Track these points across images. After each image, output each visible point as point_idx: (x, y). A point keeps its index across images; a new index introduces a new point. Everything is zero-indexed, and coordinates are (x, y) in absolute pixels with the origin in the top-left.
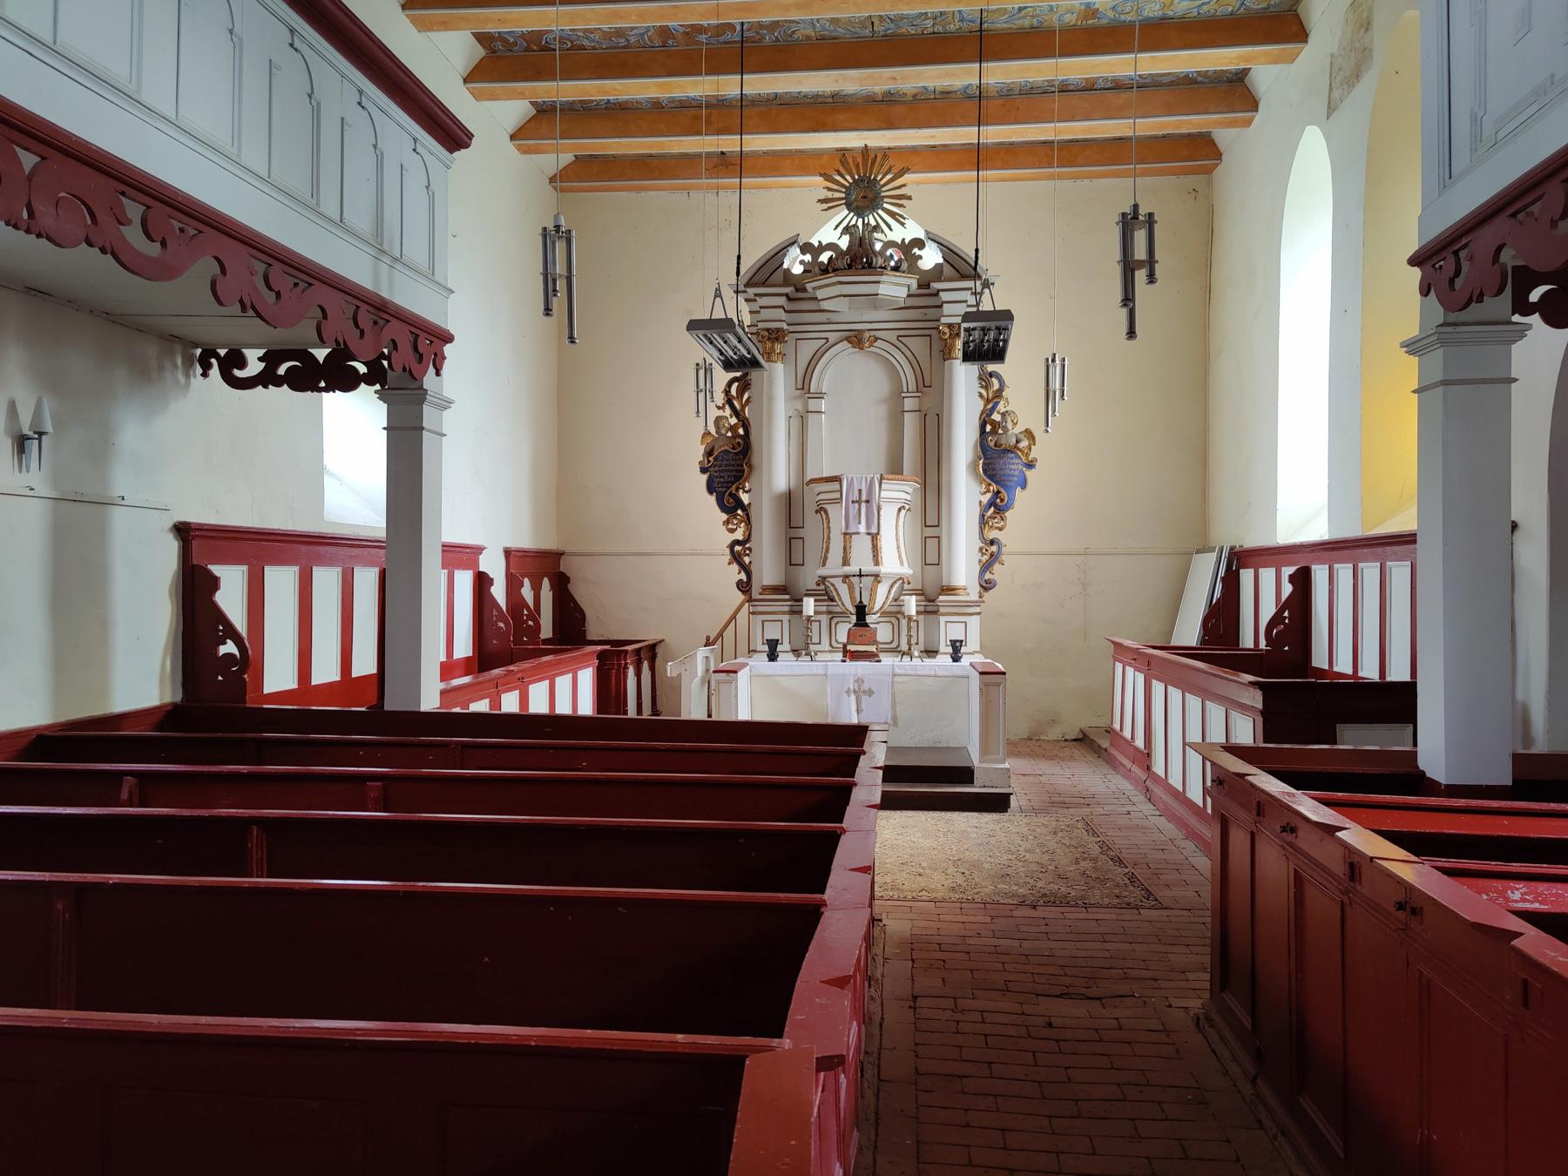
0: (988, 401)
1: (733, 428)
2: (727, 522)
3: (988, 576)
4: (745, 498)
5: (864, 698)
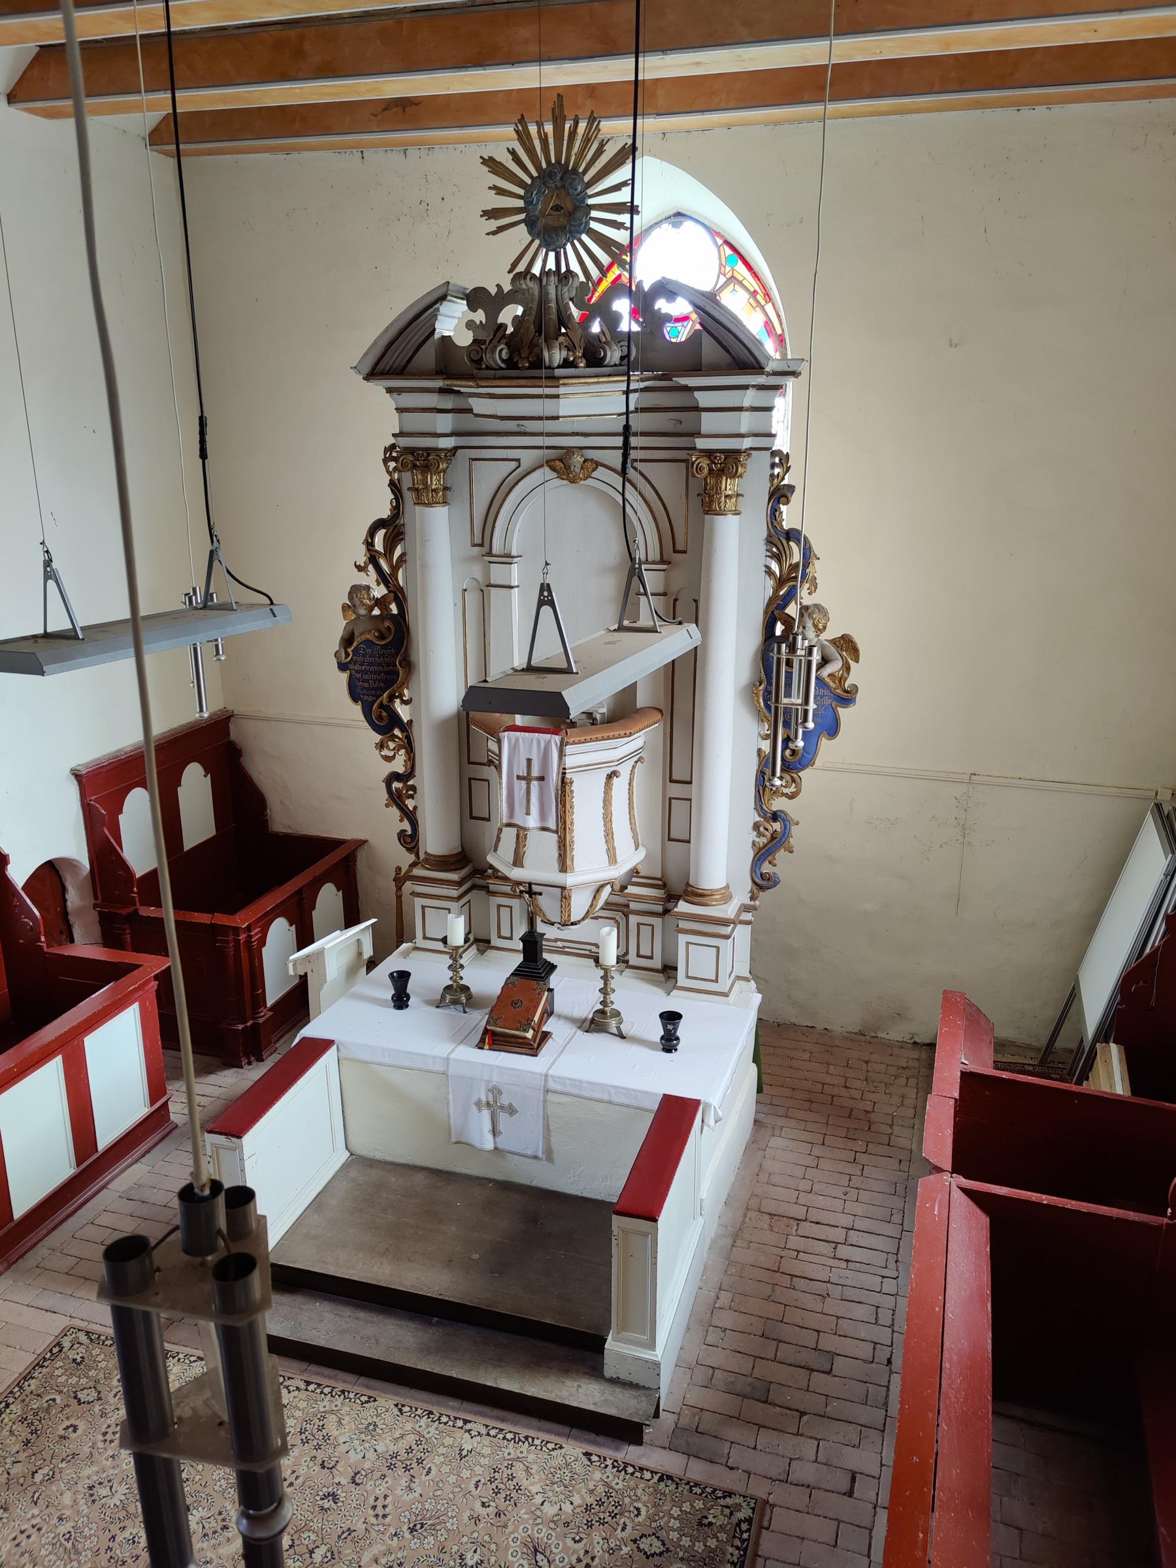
0: (781, 582)
1: (381, 603)
2: (381, 746)
3: (766, 868)
4: (404, 712)
5: (503, 1117)
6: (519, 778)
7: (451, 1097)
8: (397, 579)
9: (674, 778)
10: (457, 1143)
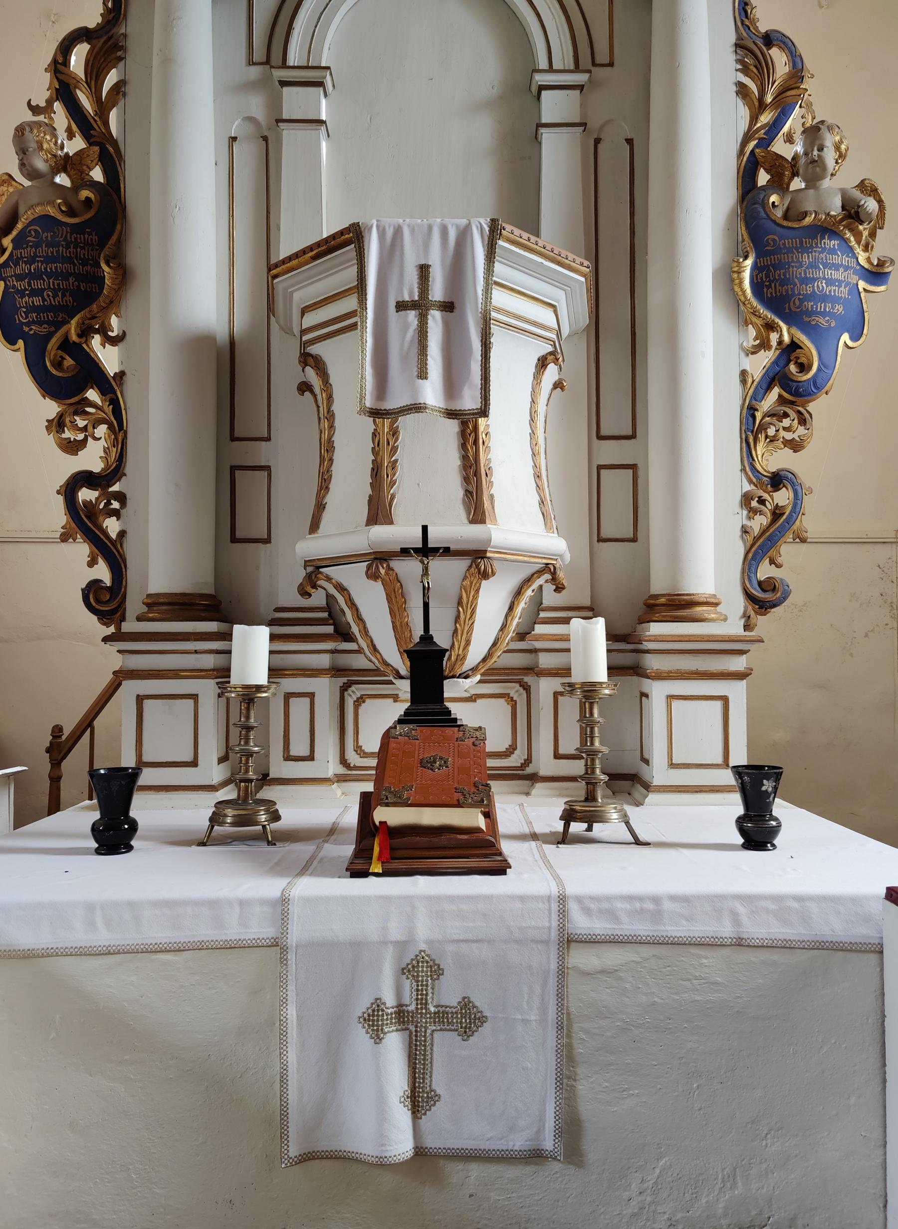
2: (57, 425)
3: (765, 571)
4: (109, 358)
5: (444, 1045)
6: (401, 306)
7: (292, 1012)
8: (106, 123)
9: (603, 432)
10: (307, 1158)
